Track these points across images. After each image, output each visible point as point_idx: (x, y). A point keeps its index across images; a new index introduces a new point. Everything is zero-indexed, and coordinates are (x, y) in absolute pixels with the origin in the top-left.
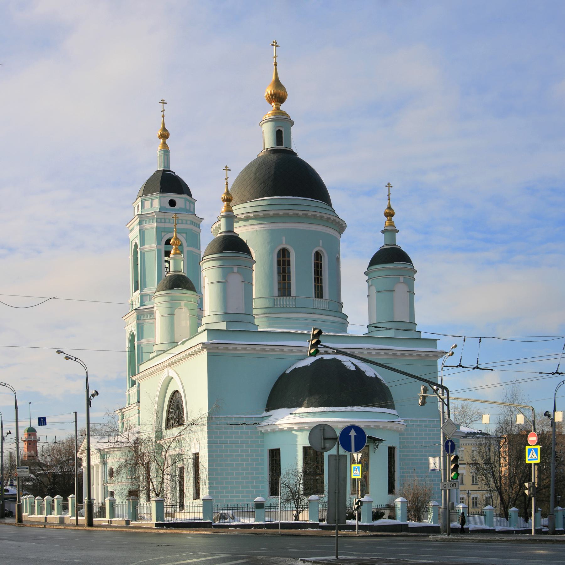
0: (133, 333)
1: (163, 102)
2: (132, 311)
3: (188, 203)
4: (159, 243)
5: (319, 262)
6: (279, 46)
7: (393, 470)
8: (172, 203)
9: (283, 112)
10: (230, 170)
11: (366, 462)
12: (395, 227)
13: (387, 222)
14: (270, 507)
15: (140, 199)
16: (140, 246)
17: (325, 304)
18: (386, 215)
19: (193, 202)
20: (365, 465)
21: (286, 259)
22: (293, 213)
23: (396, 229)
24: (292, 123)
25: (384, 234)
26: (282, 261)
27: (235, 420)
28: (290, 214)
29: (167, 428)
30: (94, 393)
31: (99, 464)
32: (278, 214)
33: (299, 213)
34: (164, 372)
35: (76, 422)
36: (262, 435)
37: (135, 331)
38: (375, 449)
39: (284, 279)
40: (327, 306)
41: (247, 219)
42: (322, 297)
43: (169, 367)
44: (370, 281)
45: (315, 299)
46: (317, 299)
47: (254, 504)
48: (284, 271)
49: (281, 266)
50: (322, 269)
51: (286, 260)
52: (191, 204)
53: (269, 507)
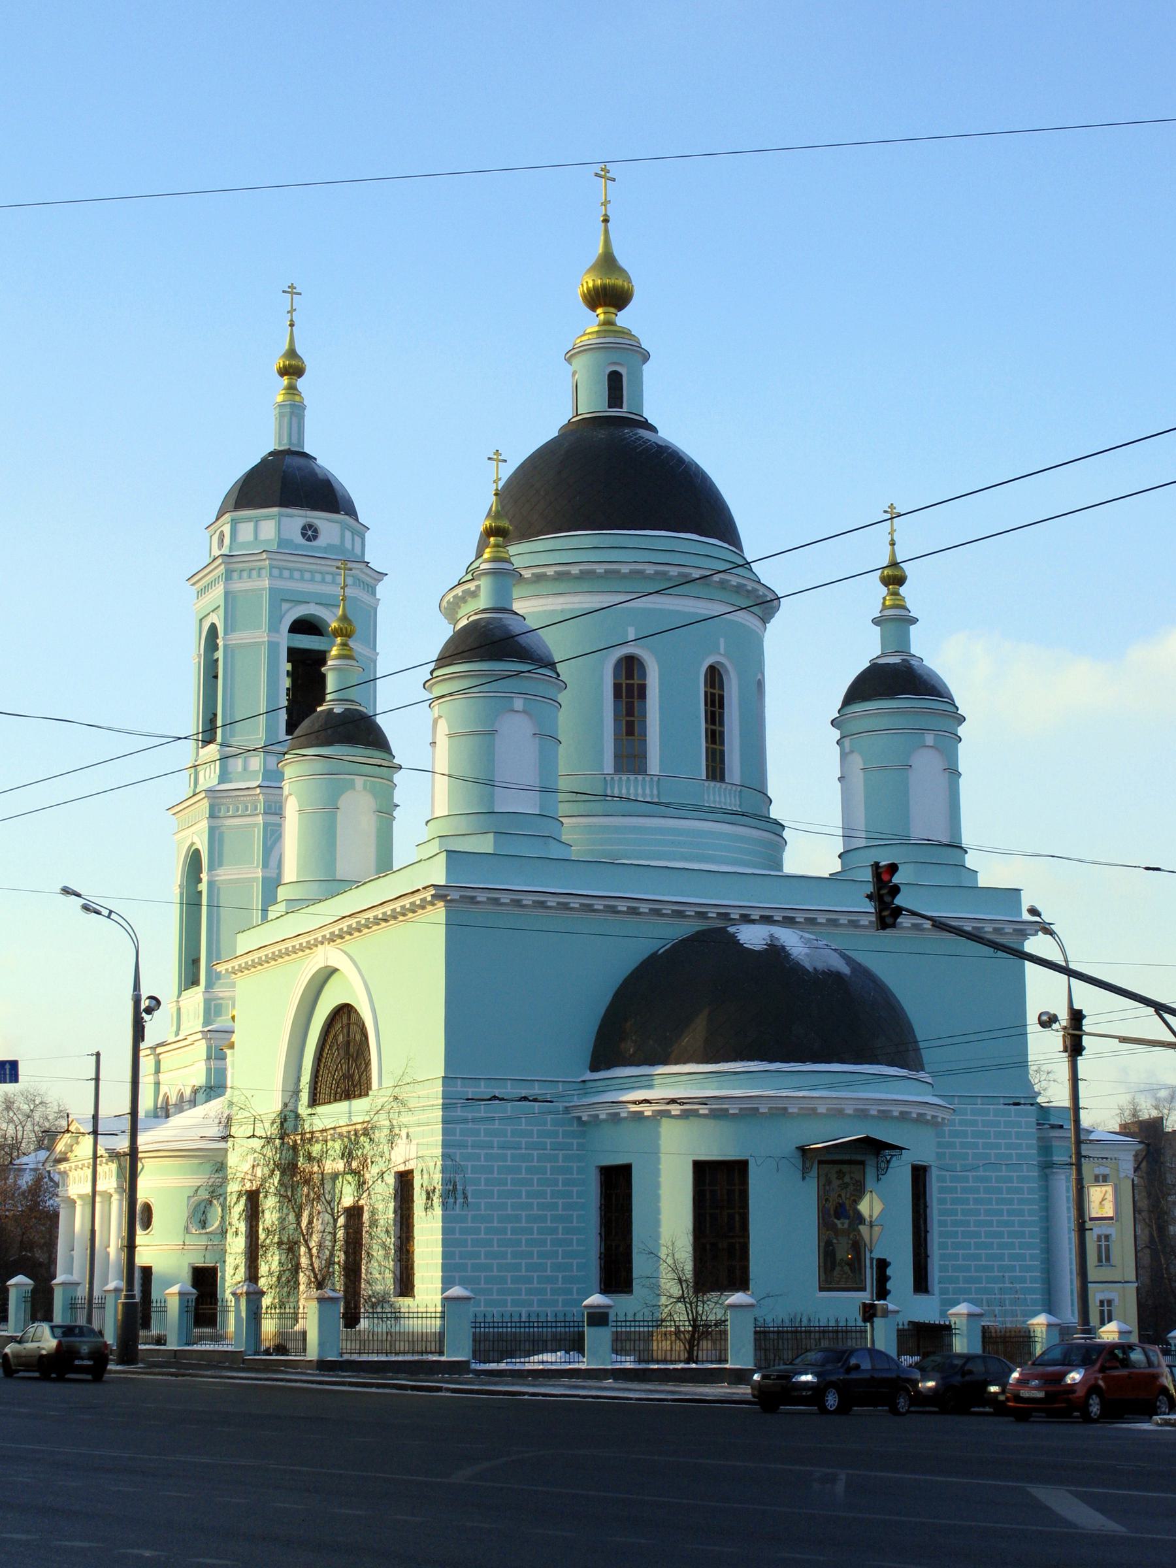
0: (197, 852)
1: (292, 291)
2: (194, 795)
3: (348, 534)
4: (273, 628)
5: (717, 691)
6: (614, 180)
7: (923, 1229)
8: (311, 534)
9: (625, 331)
12: (908, 610)
13: (888, 598)
15: (227, 517)
16: (226, 633)
17: (733, 795)
18: (887, 581)
19: (360, 532)
21: (636, 681)
22: (679, 573)
23: (910, 614)
24: (646, 357)
25: (879, 628)
26: (624, 685)
27: (485, 1087)
28: (598, 571)
29: (314, 1102)
30: (149, 1003)
31: (112, 1191)
32: (618, 572)
33: (669, 571)
34: (313, 955)
35: (97, 1079)
36: (580, 1129)
37: (203, 847)
38: (881, 1171)
39: (630, 731)
40: (735, 801)
41: (539, 578)
42: (722, 779)
43: (329, 943)
44: (847, 742)
45: (706, 783)
46: (712, 784)
47: (583, 1315)
48: (630, 712)
49: (622, 698)
50: (723, 709)
51: (636, 686)
52: (355, 536)
53: (525, 1322)
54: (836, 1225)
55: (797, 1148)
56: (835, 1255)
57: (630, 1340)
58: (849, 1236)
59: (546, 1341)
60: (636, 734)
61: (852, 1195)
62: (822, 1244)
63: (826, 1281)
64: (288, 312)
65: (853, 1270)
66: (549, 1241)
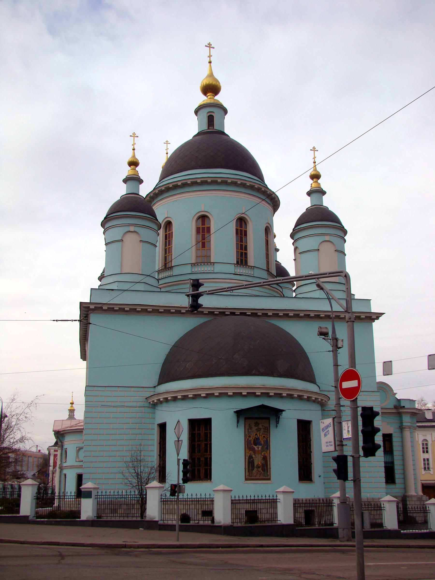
10: (138, 137)
11: (265, 439)
14: (70, 497)
20: (264, 442)
21: (206, 226)
24: (225, 111)
49: (200, 233)
54: (255, 448)
55: (234, 412)
56: (254, 463)
57: (132, 504)
58: (261, 454)
59: (128, 504)
60: (206, 247)
61: (263, 434)
62: (247, 458)
63: (249, 475)
64: (166, 150)
65: (263, 470)
66: (207, 467)
